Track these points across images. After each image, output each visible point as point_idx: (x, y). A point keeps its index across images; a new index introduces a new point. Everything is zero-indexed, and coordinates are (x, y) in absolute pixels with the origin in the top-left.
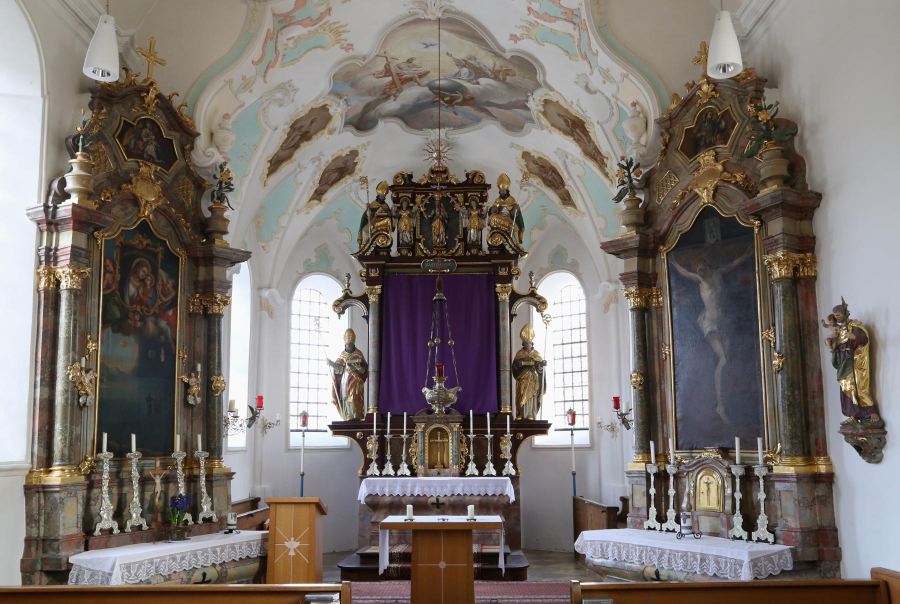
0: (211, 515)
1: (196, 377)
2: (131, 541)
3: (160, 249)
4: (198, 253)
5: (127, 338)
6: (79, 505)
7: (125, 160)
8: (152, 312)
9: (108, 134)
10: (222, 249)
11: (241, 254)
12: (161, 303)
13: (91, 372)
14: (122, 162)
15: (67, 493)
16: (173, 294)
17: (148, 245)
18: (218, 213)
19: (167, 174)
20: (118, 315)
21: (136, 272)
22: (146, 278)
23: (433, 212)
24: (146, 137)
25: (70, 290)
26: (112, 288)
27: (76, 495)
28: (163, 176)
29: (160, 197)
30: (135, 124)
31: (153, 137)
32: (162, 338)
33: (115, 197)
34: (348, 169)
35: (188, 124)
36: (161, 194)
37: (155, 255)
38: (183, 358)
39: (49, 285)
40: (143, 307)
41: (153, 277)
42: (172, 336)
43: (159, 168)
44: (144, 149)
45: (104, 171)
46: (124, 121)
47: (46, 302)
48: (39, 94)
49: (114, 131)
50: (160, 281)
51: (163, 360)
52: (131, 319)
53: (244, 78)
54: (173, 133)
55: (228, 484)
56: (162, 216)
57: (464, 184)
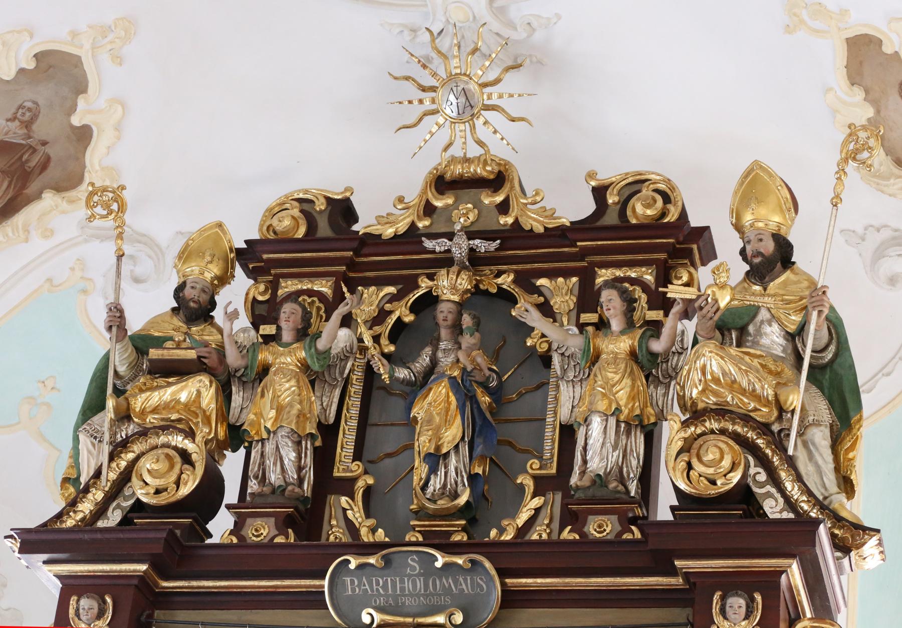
23: (425, 360)
34: (45, 165)
57: (581, 228)
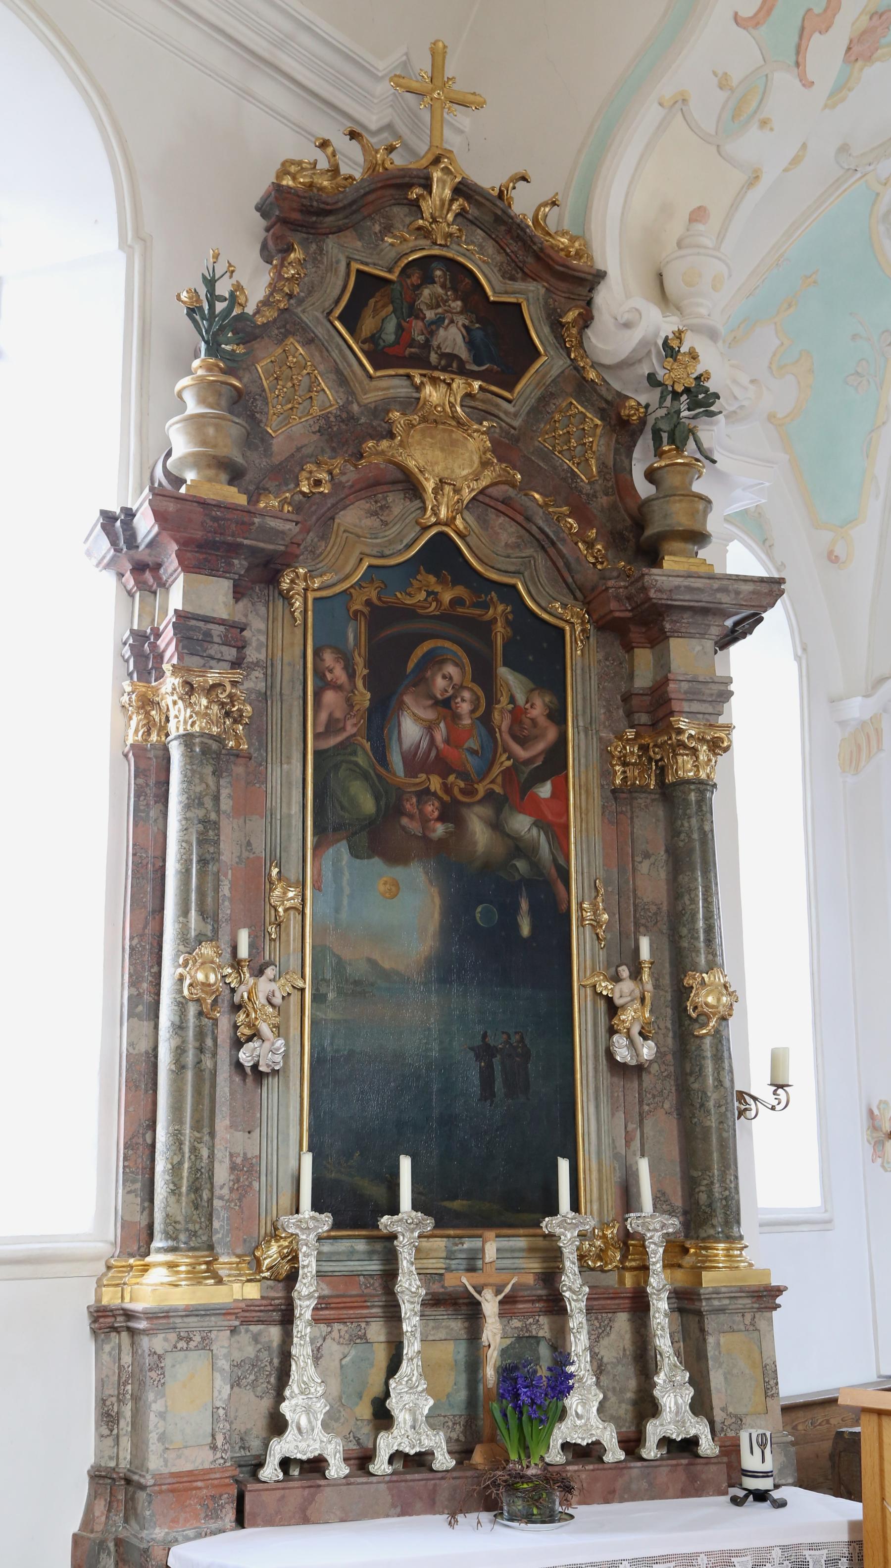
0: (693, 1432)
1: (636, 974)
2: (394, 1506)
3: (499, 610)
4: (613, 605)
5: (398, 872)
6: (217, 1375)
7: (370, 377)
8: (481, 793)
9: (310, 315)
10: (677, 581)
11: (748, 587)
12: (509, 763)
13: (270, 972)
14: (361, 383)
15: (173, 1337)
16: (552, 734)
17: (457, 602)
18: (672, 480)
19: (509, 401)
20: (368, 804)
21: (420, 680)
22: (454, 697)
24: (430, 307)
25: (187, 739)
26: (344, 729)
27: (206, 1345)
28: (497, 406)
29: (485, 464)
30: (393, 277)
31: (458, 305)
32: (521, 865)
33: (344, 479)
35: (568, 255)
36: (489, 455)
37: (484, 629)
38: (596, 924)
39: (148, 733)
40: (452, 778)
41: (481, 693)
42: (555, 860)
43: (476, 384)
44: (427, 341)
45: (308, 414)
46: (359, 272)
47: (141, 781)
48: (113, 242)
49: (328, 304)
50: (504, 700)
51: (525, 930)
52: (411, 817)
53: (723, 83)
54: (519, 285)
55: (762, 1324)
56: (502, 519)
